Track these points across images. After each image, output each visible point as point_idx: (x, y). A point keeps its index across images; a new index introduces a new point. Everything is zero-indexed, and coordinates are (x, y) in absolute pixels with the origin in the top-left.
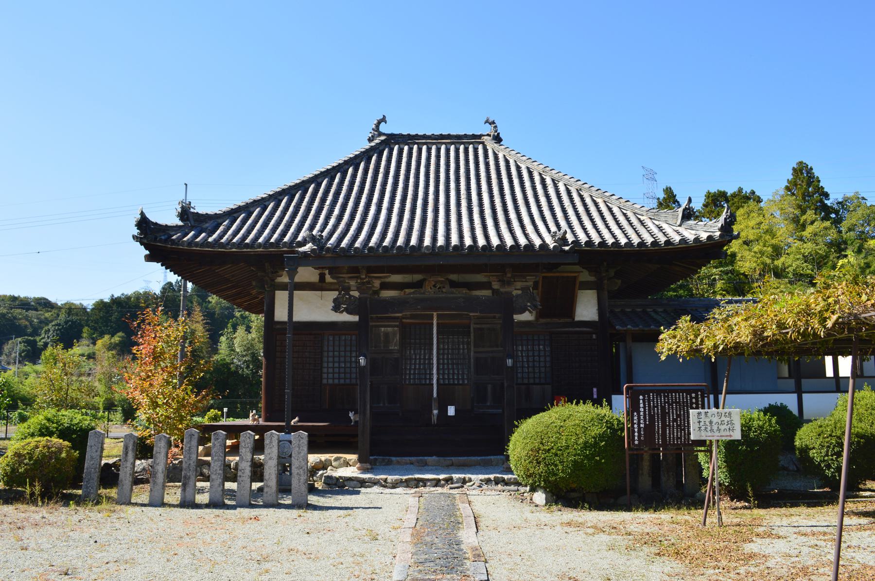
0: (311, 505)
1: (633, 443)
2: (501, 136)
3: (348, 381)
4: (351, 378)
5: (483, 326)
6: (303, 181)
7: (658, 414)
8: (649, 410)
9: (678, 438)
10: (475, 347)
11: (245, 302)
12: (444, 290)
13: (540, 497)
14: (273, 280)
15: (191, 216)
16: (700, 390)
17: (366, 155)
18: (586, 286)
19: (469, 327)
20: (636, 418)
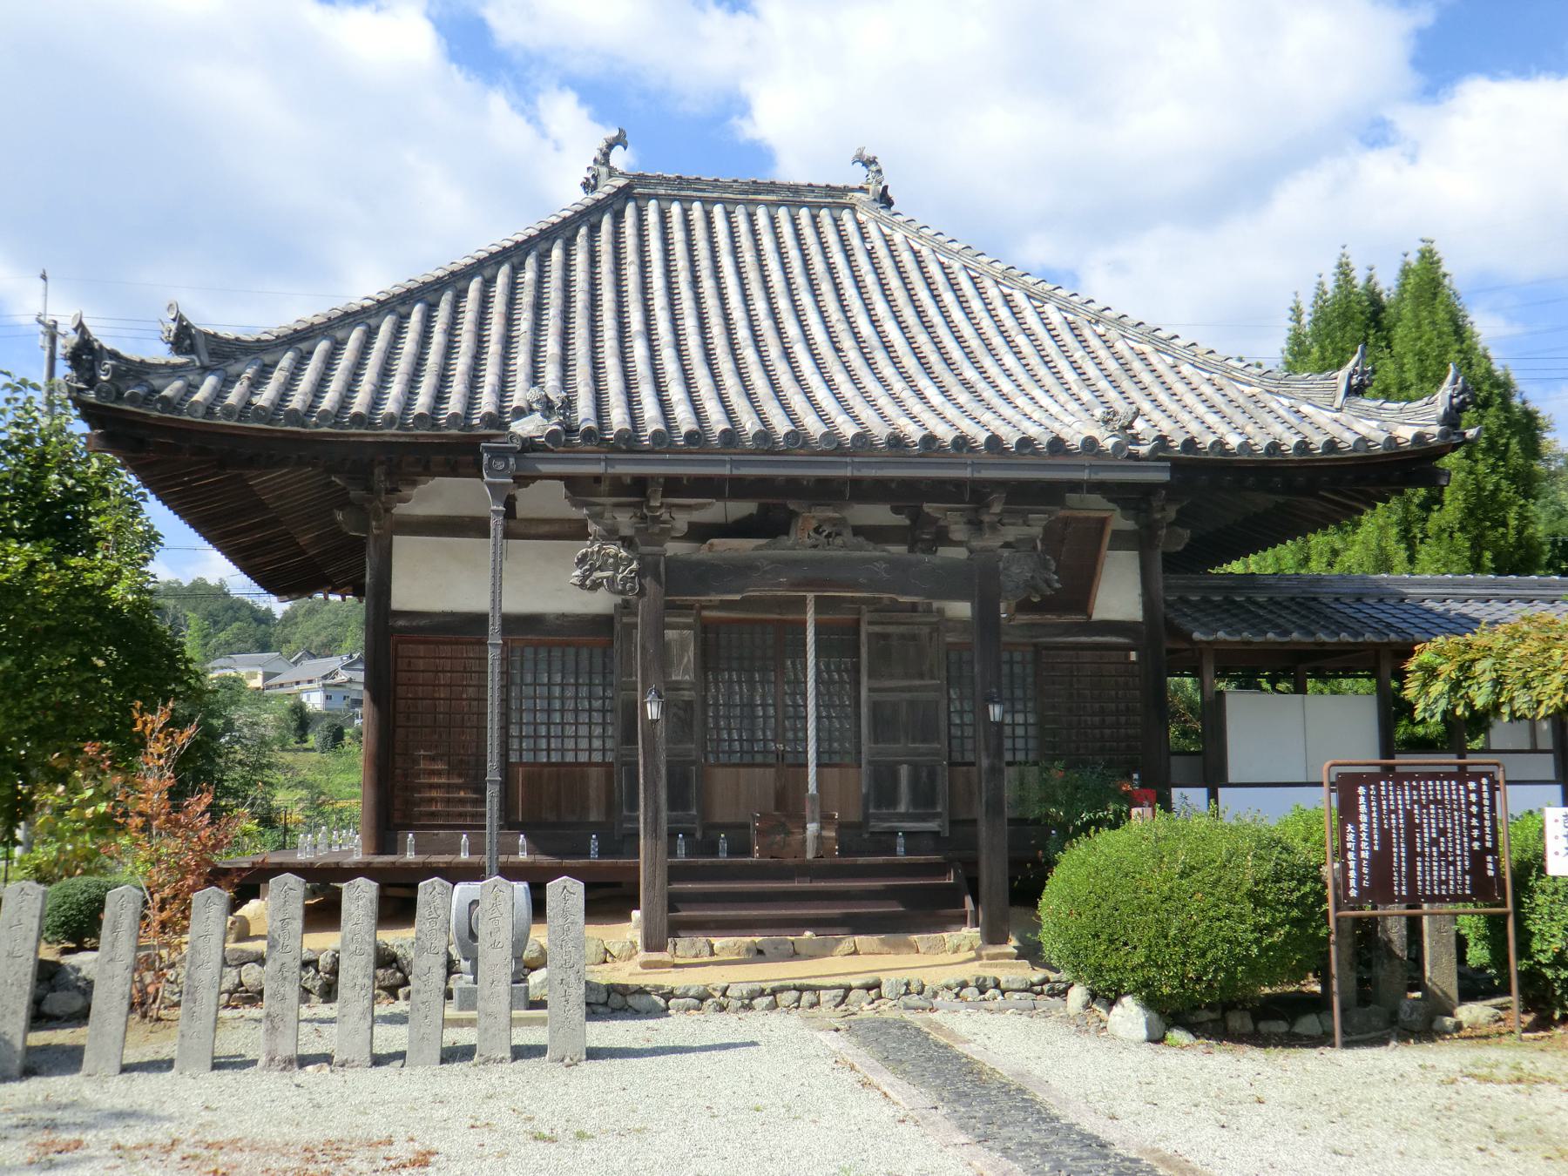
0: (383, 1056)
1: (1346, 895)
2: (890, 192)
3: (570, 758)
4: (590, 750)
5: (890, 629)
6: (452, 273)
7: (1398, 829)
8: (1380, 820)
9: (1441, 882)
10: (870, 677)
11: (267, 564)
12: (839, 541)
13: (1129, 1016)
14: (388, 510)
15: (200, 343)
16: (1485, 774)
17: (588, 217)
18: (1121, 541)
19: (857, 632)
20: (1350, 837)
